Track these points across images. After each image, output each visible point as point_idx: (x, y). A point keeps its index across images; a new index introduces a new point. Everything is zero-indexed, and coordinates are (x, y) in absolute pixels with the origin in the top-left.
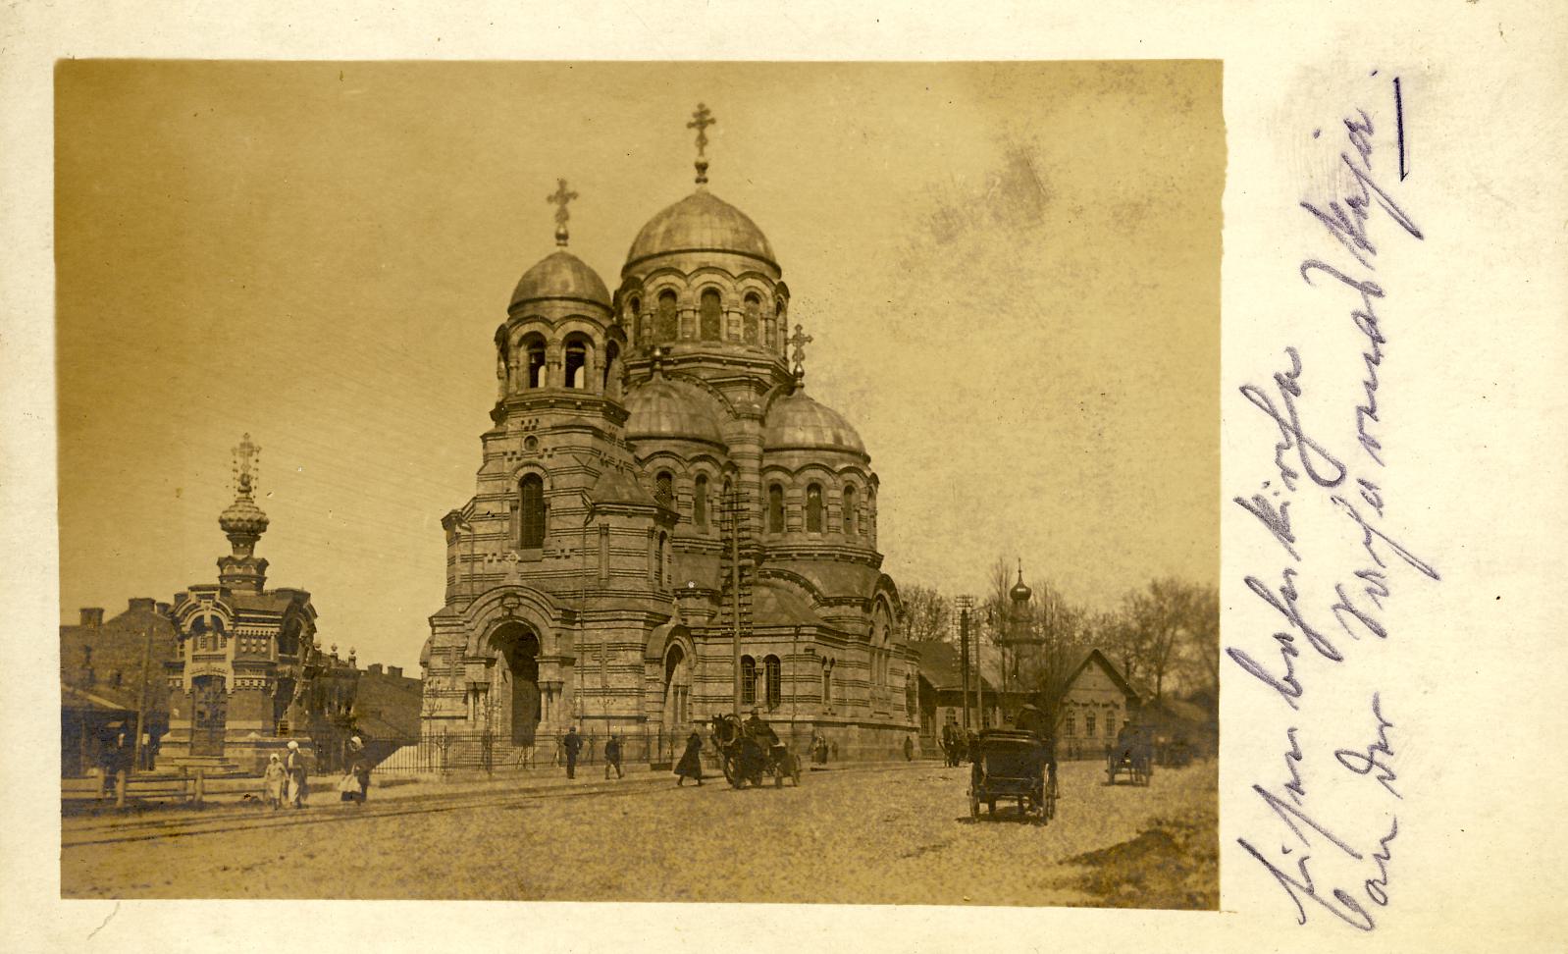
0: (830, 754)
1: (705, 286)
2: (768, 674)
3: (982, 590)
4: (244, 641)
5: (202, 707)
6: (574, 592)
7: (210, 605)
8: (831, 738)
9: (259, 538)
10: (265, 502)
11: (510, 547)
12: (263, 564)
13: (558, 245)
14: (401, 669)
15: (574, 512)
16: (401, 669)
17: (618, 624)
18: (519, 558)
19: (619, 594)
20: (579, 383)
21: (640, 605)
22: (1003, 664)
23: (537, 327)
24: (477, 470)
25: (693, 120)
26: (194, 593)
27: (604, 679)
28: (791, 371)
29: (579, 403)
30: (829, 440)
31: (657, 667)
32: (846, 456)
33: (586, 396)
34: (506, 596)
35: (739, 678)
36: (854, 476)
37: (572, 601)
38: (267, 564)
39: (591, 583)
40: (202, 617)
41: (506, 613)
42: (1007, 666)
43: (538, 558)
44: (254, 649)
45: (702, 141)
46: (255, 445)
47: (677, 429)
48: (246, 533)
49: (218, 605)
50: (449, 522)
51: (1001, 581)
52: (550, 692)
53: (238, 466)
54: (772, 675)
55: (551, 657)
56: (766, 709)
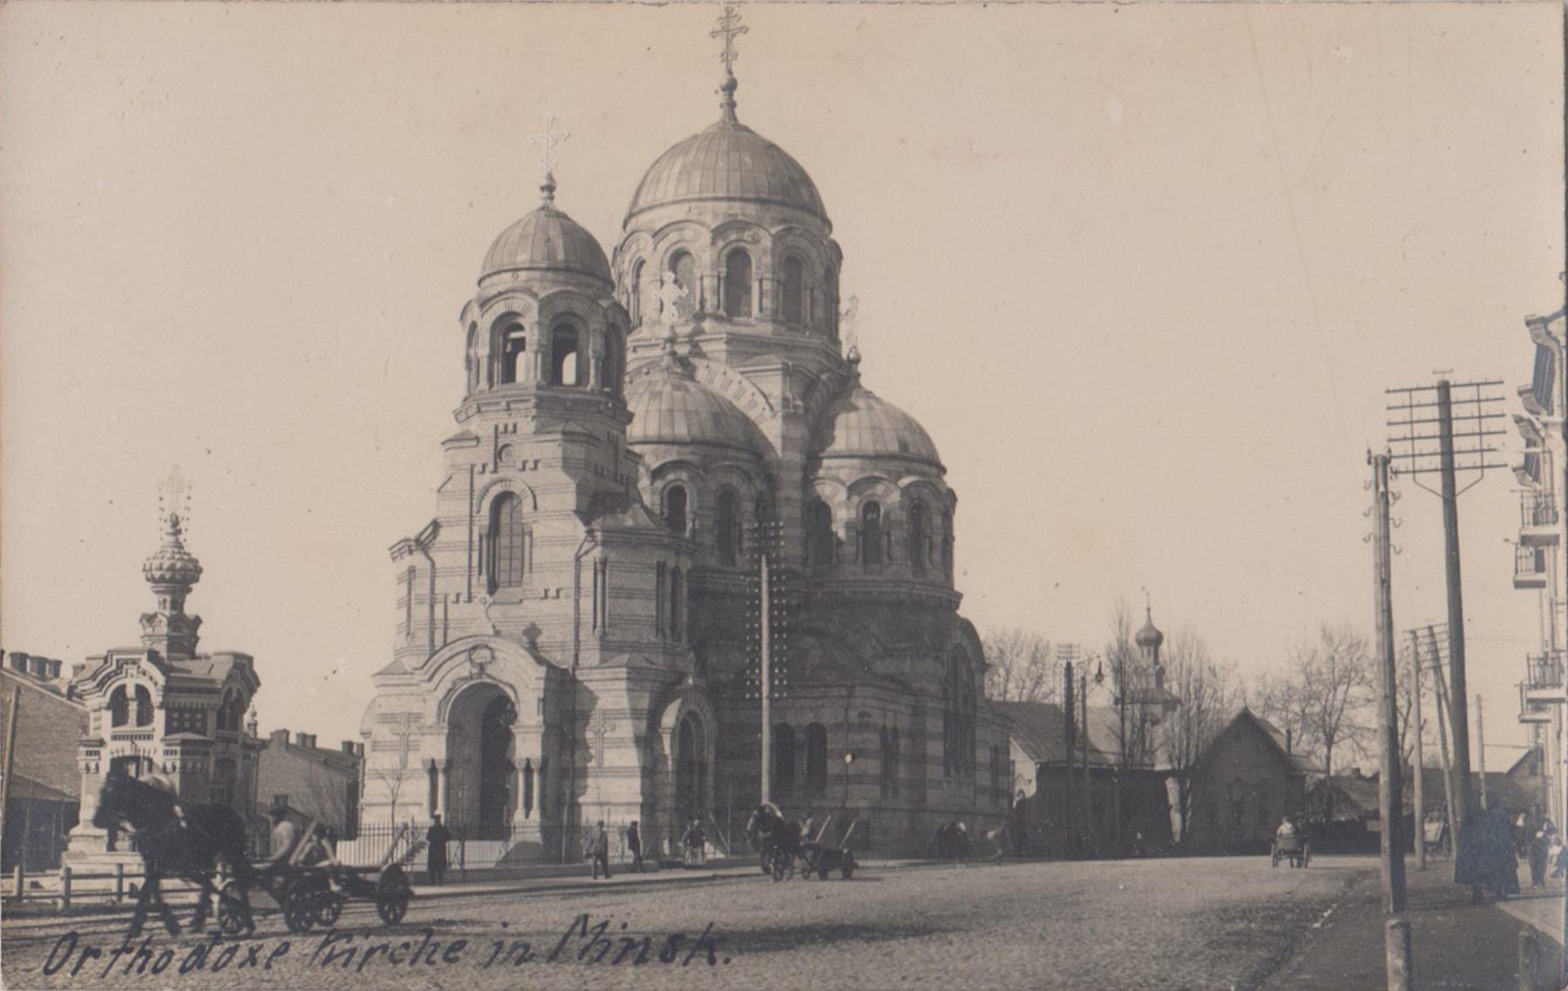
3: (1094, 639)
4: (176, 715)
9: (190, 590)
10: (195, 546)
14: (314, 737)
16: (314, 737)
25: (718, 27)
28: (844, 356)
34: (475, 648)
40: (123, 687)
42: (1128, 733)
47: (696, 432)
48: (179, 579)
53: (165, 504)
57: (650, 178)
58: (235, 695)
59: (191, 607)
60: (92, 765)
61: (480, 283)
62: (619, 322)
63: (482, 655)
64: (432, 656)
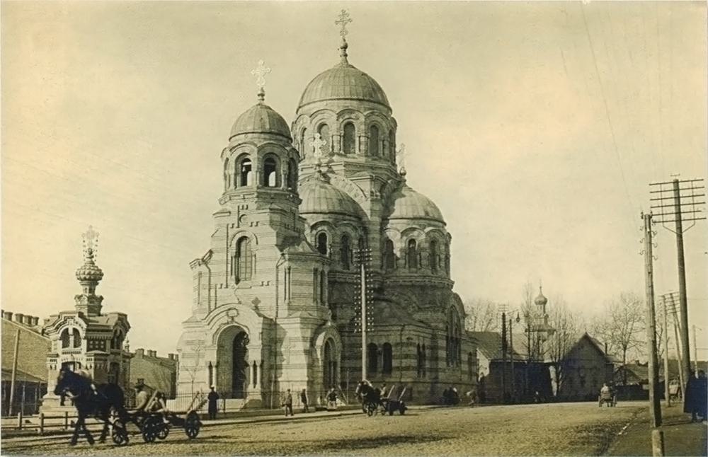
9: (97, 284)
14: (155, 352)
16: (155, 352)
20: (272, 182)
22: (529, 345)
28: (399, 172)
29: (272, 196)
40: (67, 329)
42: (531, 346)
51: (528, 294)
53: (86, 244)
58: (118, 332)
64: (210, 313)
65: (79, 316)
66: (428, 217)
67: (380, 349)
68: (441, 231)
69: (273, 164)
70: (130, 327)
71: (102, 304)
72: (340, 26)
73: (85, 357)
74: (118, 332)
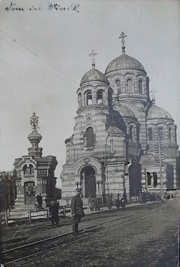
0: (171, 197)
1: (128, 78)
2: (154, 177)
4: (40, 171)
5: (27, 191)
6: (103, 158)
7: (29, 161)
8: (171, 194)
9: (39, 142)
10: (40, 131)
11: (84, 147)
12: (41, 149)
13: (93, 67)
15: (103, 136)
17: (117, 165)
18: (86, 149)
19: (117, 157)
21: (123, 160)
23: (88, 88)
24: (74, 128)
25: (121, 36)
26: (23, 158)
27: (114, 180)
29: (102, 108)
30: (165, 117)
31: (127, 176)
32: (169, 120)
33: (104, 106)
35: (147, 178)
36: (171, 126)
37: (103, 160)
38: (43, 149)
39: (108, 155)
40: (26, 165)
41: (86, 163)
43: (92, 149)
44: (42, 173)
45: (123, 42)
46: (37, 116)
48: (36, 140)
49: (31, 161)
50: (66, 141)
52: (99, 183)
54: (155, 177)
55: (99, 174)
56: (154, 186)
57: (109, 66)
58: (53, 166)
59: (40, 146)
60: (19, 184)
61: (80, 85)
62: (111, 91)
63: (87, 160)
64: (75, 162)
65: (32, 158)
66: (167, 118)
67: (19, 192)
68: (173, 124)
69: (102, 94)
70: (57, 163)
71: (42, 152)
72: (121, 39)
73: (37, 179)
74: (53, 166)
